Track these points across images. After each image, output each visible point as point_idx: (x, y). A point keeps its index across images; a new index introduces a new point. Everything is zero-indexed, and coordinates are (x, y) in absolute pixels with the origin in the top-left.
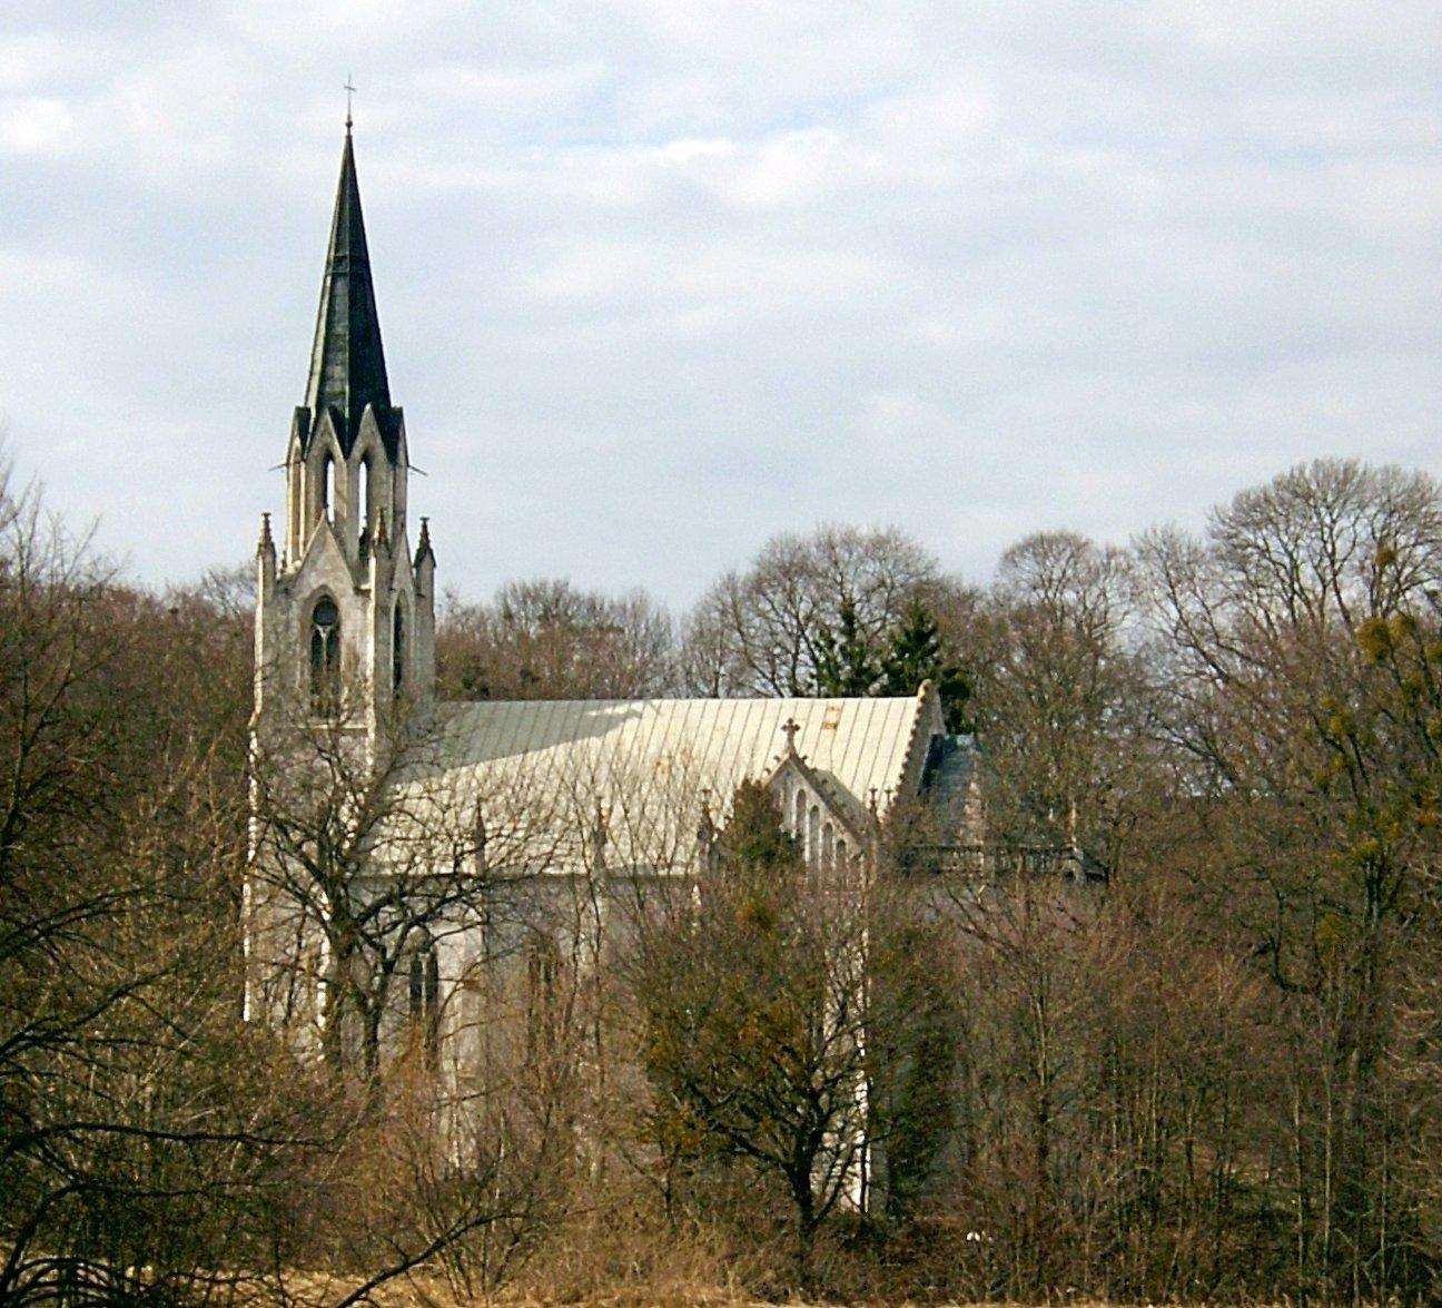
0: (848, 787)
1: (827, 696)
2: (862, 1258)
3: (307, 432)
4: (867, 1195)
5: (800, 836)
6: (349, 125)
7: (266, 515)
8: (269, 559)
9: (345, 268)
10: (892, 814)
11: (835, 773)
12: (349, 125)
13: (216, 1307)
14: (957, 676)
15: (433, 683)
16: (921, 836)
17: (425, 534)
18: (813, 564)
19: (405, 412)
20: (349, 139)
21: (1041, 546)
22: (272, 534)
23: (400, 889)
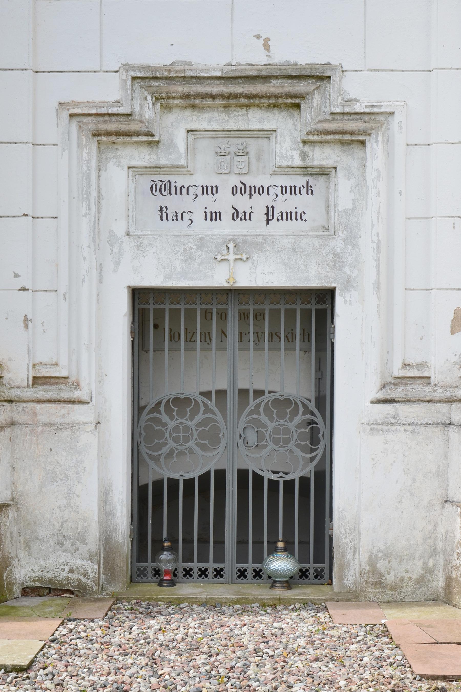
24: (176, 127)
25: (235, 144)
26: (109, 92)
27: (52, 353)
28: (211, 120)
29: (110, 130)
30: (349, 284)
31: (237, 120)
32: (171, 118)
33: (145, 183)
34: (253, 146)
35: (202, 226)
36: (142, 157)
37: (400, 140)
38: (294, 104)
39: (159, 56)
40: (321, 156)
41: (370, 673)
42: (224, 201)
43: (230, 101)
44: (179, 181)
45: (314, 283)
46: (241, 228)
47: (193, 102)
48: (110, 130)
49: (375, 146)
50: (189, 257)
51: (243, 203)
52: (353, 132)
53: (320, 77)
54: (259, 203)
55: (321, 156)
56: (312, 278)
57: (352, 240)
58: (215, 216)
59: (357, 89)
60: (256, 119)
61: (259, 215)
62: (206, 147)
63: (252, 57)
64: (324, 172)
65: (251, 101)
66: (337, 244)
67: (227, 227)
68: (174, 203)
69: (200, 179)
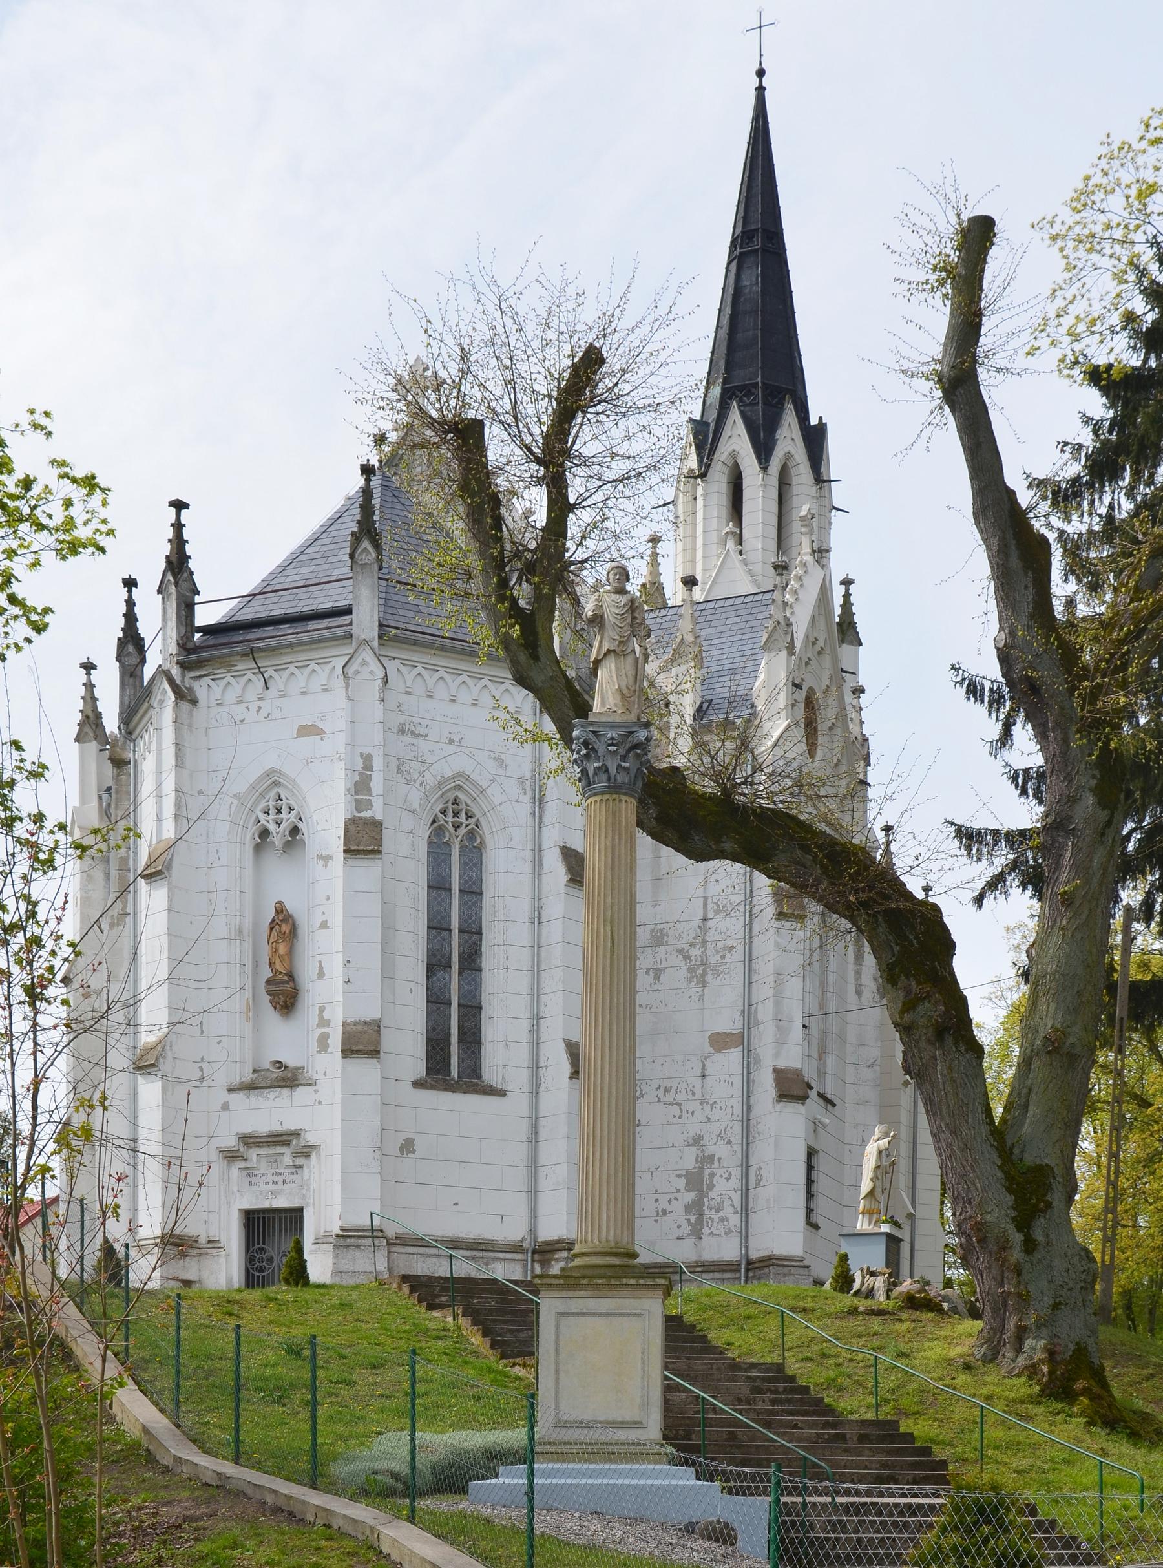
0: (756, 873)
1: (512, 1464)
2: (936, 284)
3: (706, 436)
4: (699, 554)
5: (541, 712)
6: (761, 73)
7: (179, 506)
8: (134, 660)
9: (758, 243)
10: (589, 379)
11: (604, 352)
12: (761, 73)
13: (2, 801)
14: (854, 715)
15: (1021, 1387)
16: (128, 1170)
17: (847, 596)
18: (1026, 574)
19: (247, 1206)
20: (761, 89)
21: (727, 1525)
22: (768, 94)
23: (975, 1314)
24: (253, 1154)
25: (273, 1159)
26: (231, 1143)
27: (214, 1233)
28: (264, 1151)
29: (231, 1156)
30: (308, 1205)
31: (272, 1150)
32: (251, 1150)
33: (245, 1173)
34: (279, 1159)
35: (263, 1188)
36: (242, 1165)
37: (323, 1153)
38: (287, 1144)
39: (247, 1130)
40: (299, 1161)
41: (509, 462)
42: (270, 1178)
43: (269, 1144)
44: (256, 1172)
45: (296, 1205)
46: (275, 1187)
47: (258, 1145)
48: (231, 1156)
49: (313, 1157)
50: (257, 1197)
51: (276, 1178)
52: (306, 1152)
53: (296, 1134)
54: (281, 1178)
55: (299, 1161)
56: (295, 1203)
57: (308, 1190)
58: (267, 1183)
59: (310, 1138)
60: (279, 1150)
61: (281, 1183)
62: (264, 1160)
63: (277, 1128)
64: (301, 1167)
65: (275, 1144)
66: (304, 1191)
67: (271, 1187)
68: (253, 1179)
69: (262, 1171)
